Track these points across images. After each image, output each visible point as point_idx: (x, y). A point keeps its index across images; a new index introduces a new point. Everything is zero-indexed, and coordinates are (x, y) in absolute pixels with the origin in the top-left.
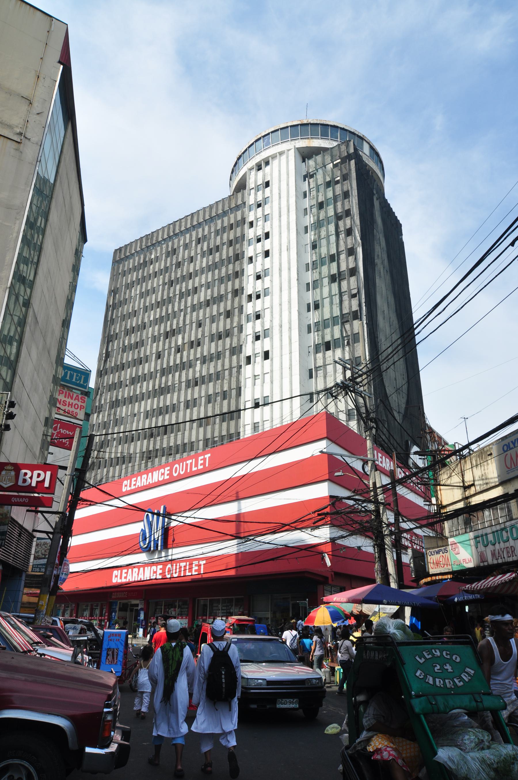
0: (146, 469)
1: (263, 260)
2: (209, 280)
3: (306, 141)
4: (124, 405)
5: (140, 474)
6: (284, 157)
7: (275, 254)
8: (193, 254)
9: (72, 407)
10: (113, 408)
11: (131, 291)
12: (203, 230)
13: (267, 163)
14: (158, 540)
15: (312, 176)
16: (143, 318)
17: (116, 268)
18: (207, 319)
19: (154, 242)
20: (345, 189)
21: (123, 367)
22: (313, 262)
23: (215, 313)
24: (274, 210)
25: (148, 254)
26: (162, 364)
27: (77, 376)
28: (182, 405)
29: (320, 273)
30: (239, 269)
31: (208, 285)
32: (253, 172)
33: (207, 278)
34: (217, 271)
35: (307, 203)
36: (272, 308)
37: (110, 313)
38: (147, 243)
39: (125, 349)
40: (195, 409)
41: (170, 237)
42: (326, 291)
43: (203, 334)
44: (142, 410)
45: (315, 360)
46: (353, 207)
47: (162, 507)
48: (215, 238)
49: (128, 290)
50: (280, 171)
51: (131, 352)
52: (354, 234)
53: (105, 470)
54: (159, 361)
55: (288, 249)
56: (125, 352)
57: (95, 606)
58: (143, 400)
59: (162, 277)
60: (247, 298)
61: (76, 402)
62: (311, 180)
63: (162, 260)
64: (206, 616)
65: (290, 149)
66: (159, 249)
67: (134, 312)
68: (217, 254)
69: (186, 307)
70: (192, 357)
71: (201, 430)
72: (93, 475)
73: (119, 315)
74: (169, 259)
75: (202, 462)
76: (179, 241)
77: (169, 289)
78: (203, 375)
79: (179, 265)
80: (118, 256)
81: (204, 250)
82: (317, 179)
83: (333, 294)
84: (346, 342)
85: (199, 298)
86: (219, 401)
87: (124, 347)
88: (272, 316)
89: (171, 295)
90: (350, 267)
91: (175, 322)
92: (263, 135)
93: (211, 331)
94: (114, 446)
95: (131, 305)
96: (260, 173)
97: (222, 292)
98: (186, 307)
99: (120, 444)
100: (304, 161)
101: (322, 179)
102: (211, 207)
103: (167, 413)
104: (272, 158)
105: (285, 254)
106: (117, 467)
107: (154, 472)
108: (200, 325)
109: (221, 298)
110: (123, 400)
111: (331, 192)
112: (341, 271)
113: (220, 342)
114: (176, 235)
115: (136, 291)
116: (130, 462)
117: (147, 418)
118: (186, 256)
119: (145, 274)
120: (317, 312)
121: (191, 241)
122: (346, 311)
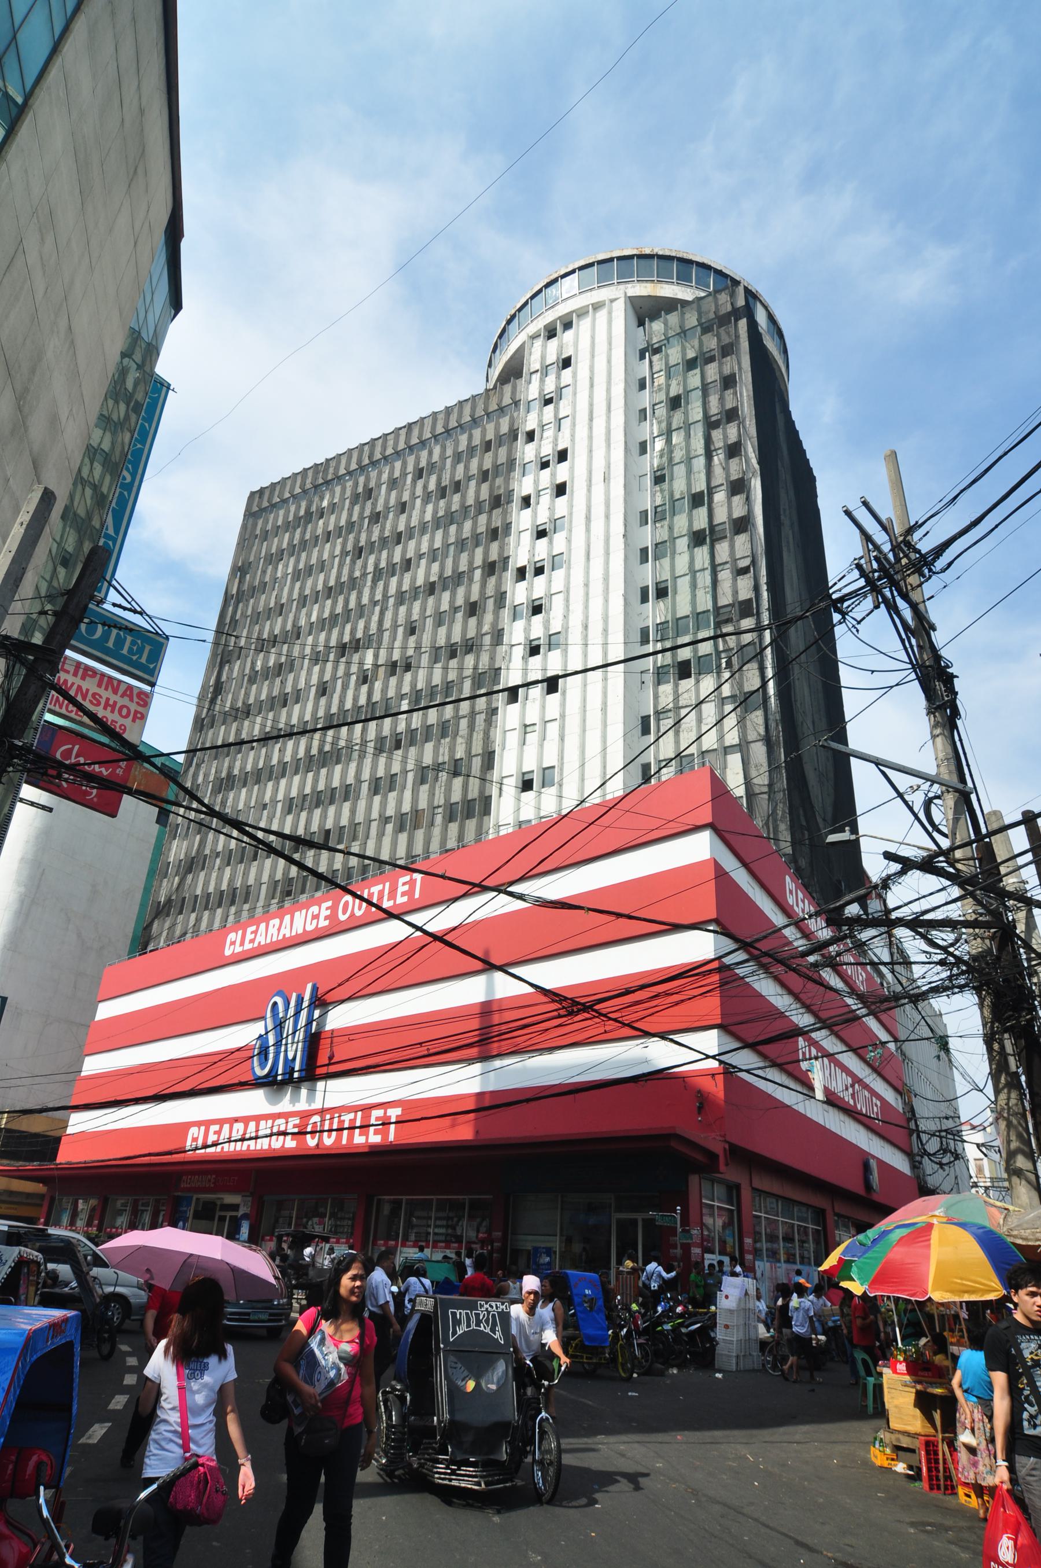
0: (282, 907)
1: (553, 502)
2: (438, 544)
3: (649, 285)
4: (244, 786)
5: (267, 917)
6: (602, 315)
7: (578, 489)
8: (406, 497)
9: (113, 711)
10: (220, 792)
11: (277, 568)
12: (430, 453)
13: (568, 325)
14: (294, 1058)
15: (657, 351)
16: (296, 619)
17: (249, 526)
18: (428, 620)
19: (330, 477)
20: (727, 371)
21: (246, 712)
22: (656, 507)
23: (445, 606)
24: (578, 409)
25: (316, 499)
26: (329, 706)
27: (133, 643)
28: (365, 787)
29: (671, 528)
30: (499, 524)
31: (433, 555)
32: (538, 343)
33: (432, 540)
34: (453, 529)
35: (645, 399)
36: (568, 592)
37: (231, 609)
38: (315, 478)
39: (256, 677)
40: (392, 796)
41: (362, 468)
42: (682, 563)
43: (418, 648)
44: (280, 796)
45: (656, 697)
46: (742, 405)
47: (309, 986)
48: (454, 467)
49: (270, 567)
50: (593, 338)
51: (267, 683)
52: (746, 452)
53: (193, 916)
54: (323, 701)
55: (606, 479)
56: (254, 683)
57: (143, 1205)
58: (283, 776)
59: (340, 540)
60: (515, 573)
61: (125, 701)
62: (656, 358)
63: (343, 509)
64: (397, 1240)
65: (616, 299)
66: (338, 489)
67: (279, 606)
68: (456, 498)
69: (385, 597)
70: (391, 693)
71: (403, 837)
72: (167, 925)
73: (249, 613)
74: (357, 508)
75: (406, 888)
76: (380, 474)
77: (353, 562)
78: (414, 726)
79: (376, 517)
80: (255, 503)
81: (430, 490)
82: (667, 356)
83: (697, 568)
84: (724, 661)
85: (414, 579)
86: (444, 778)
87: (253, 673)
88: (567, 606)
89: (357, 574)
90: (736, 515)
91: (361, 624)
92: (562, 272)
93: (434, 640)
94: (216, 867)
95: (275, 593)
96: (553, 343)
97: (463, 567)
98: (385, 597)
99: (228, 864)
100: (641, 323)
101: (679, 355)
102: (448, 410)
103: (331, 803)
104: (578, 316)
105: (598, 489)
106: (219, 911)
107: (297, 914)
108: (412, 631)
109: (458, 578)
110: (243, 776)
111: (698, 377)
112: (715, 523)
113: (453, 663)
114: (373, 463)
115: (286, 568)
116: (246, 901)
117: (289, 812)
118: (392, 501)
119: (307, 537)
120: (661, 603)
121: (404, 474)
122: (725, 599)
